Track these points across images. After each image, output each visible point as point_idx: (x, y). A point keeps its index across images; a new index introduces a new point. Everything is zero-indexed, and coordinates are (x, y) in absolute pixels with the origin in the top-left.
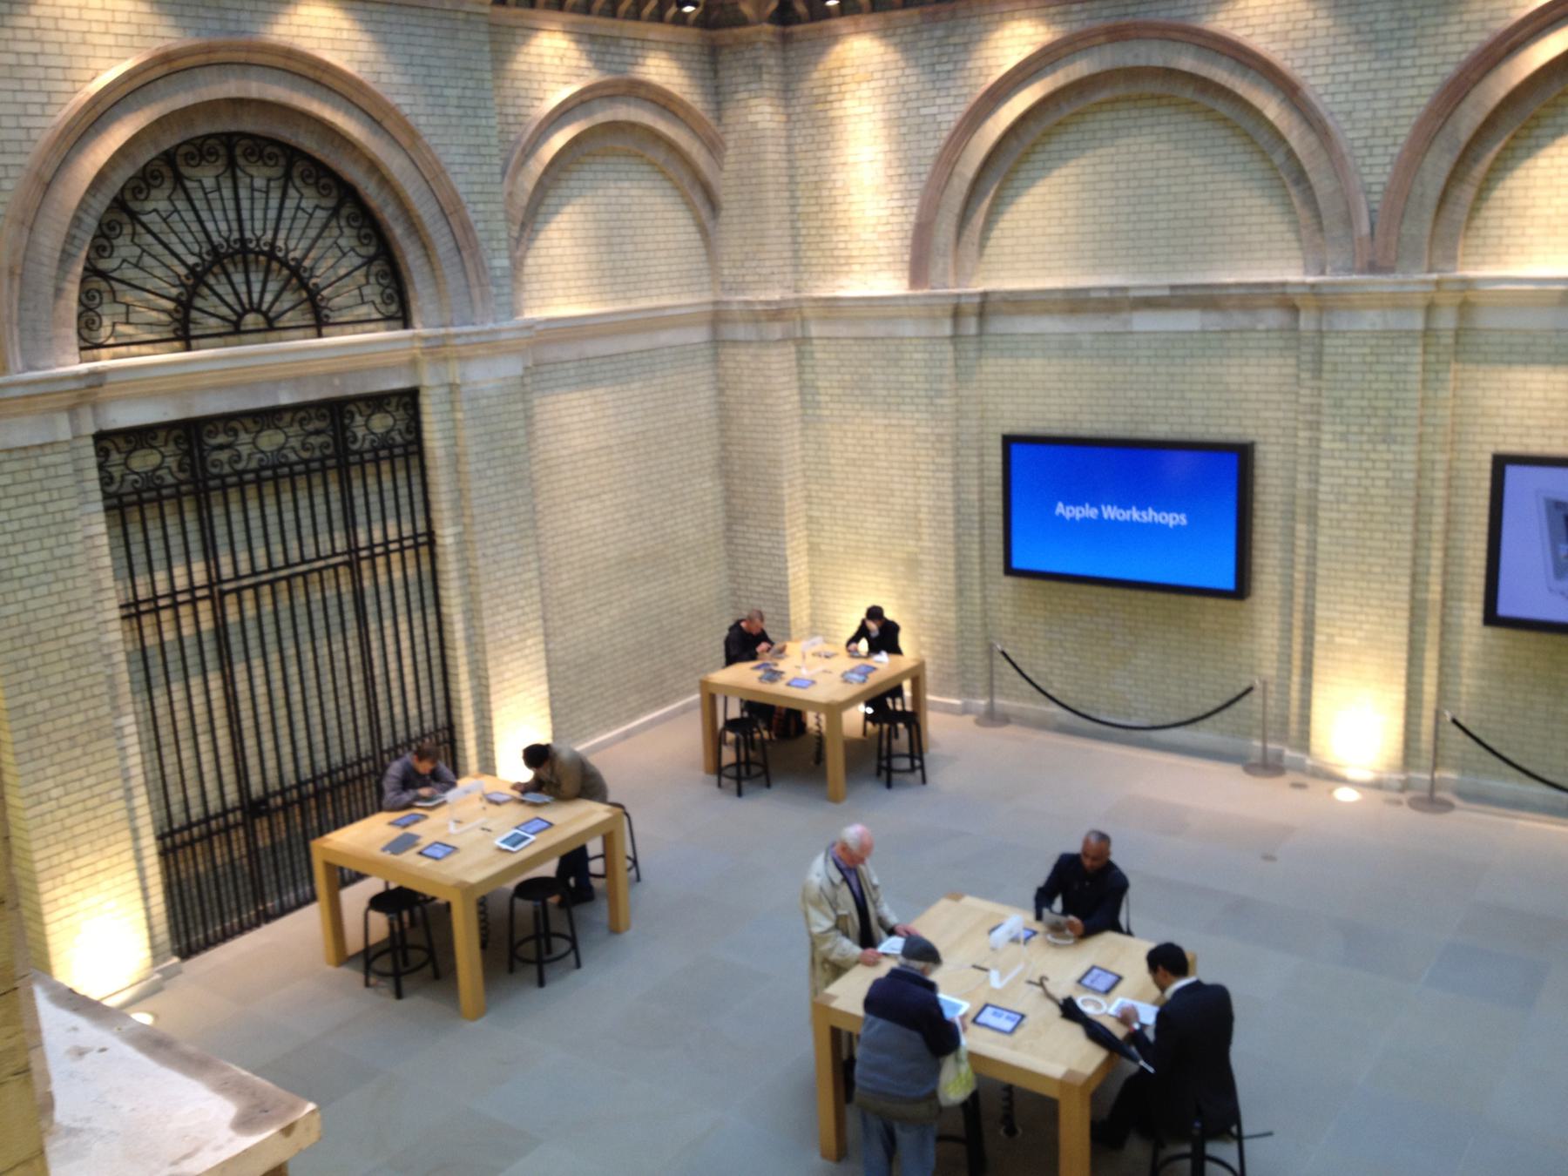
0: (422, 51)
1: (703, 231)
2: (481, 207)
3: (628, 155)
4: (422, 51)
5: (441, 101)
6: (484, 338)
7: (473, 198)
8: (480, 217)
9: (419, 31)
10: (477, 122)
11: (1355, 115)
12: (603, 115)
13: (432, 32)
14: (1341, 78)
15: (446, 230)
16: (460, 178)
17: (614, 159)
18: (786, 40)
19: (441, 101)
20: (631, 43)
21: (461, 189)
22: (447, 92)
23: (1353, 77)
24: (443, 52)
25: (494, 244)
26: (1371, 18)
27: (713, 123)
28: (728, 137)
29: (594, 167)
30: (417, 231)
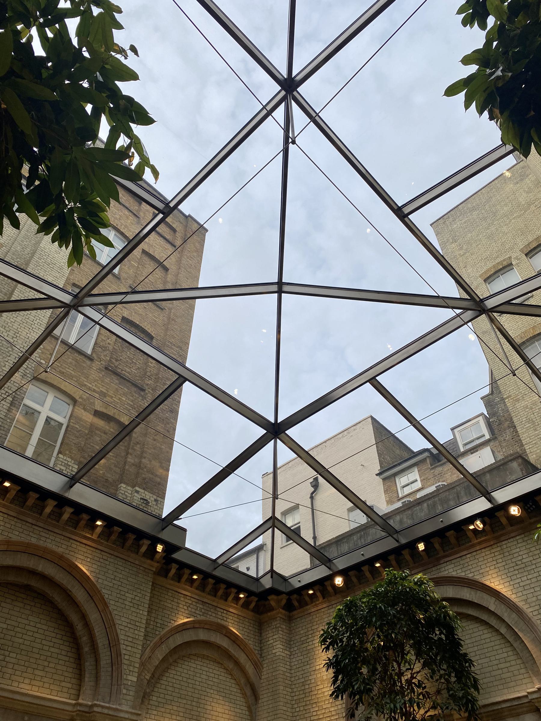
0: (121, 576)
1: (250, 710)
2: (129, 648)
3: (215, 661)
4: (121, 576)
5: (123, 597)
6: (111, 713)
7: (126, 643)
8: (128, 653)
9: (121, 568)
10: (138, 611)
11: (529, 601)
12: (202, 635)
13: (128, 570)
14: (517, 585)
15: (109, 653)
16: (123, 632)
17: (208, 662)
18: (290, 620)
19: (123, 597)
20: (222, 611)
21: (121, 637)
22: (127, 595)
23: (521, 584)
24: (130, 579)
25: (131, 668)
26: (520, 558)
27: (259, 656)
28: (264, 662)
29: (197, 662)
30: (95, 653)
